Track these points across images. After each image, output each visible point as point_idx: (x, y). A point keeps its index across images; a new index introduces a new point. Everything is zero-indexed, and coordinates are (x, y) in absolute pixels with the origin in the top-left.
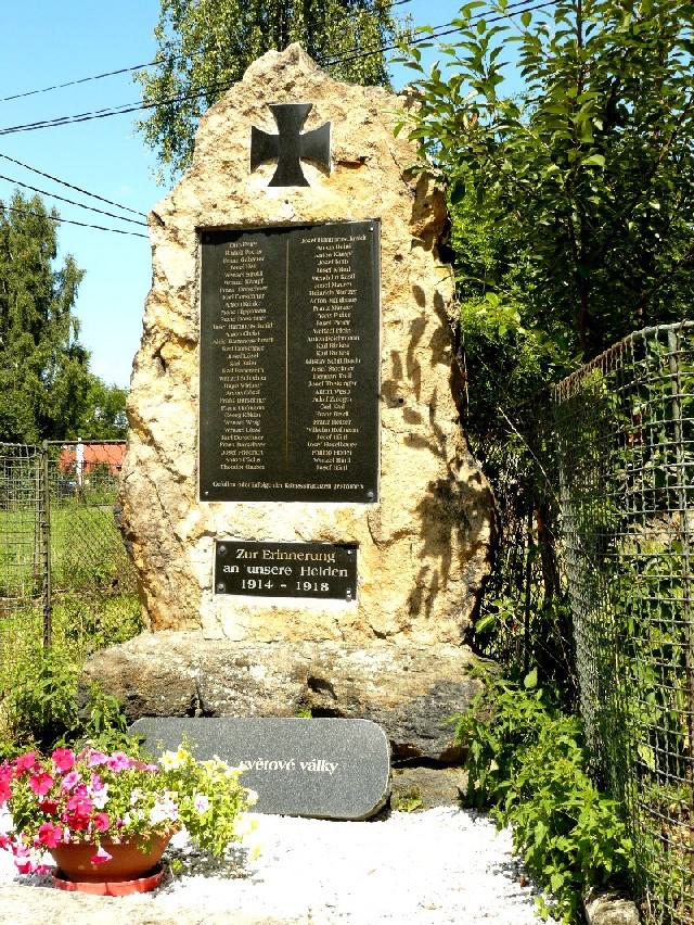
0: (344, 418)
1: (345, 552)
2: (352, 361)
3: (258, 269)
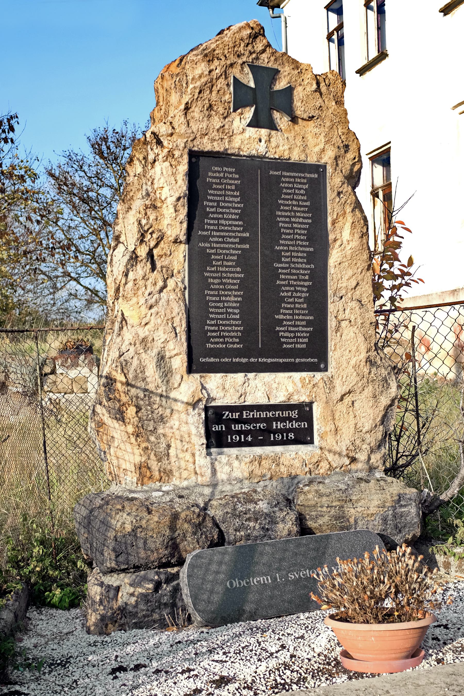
0: (303, 309)
1: (304, 411)
2: (309, 266)
3: (236, 190)
